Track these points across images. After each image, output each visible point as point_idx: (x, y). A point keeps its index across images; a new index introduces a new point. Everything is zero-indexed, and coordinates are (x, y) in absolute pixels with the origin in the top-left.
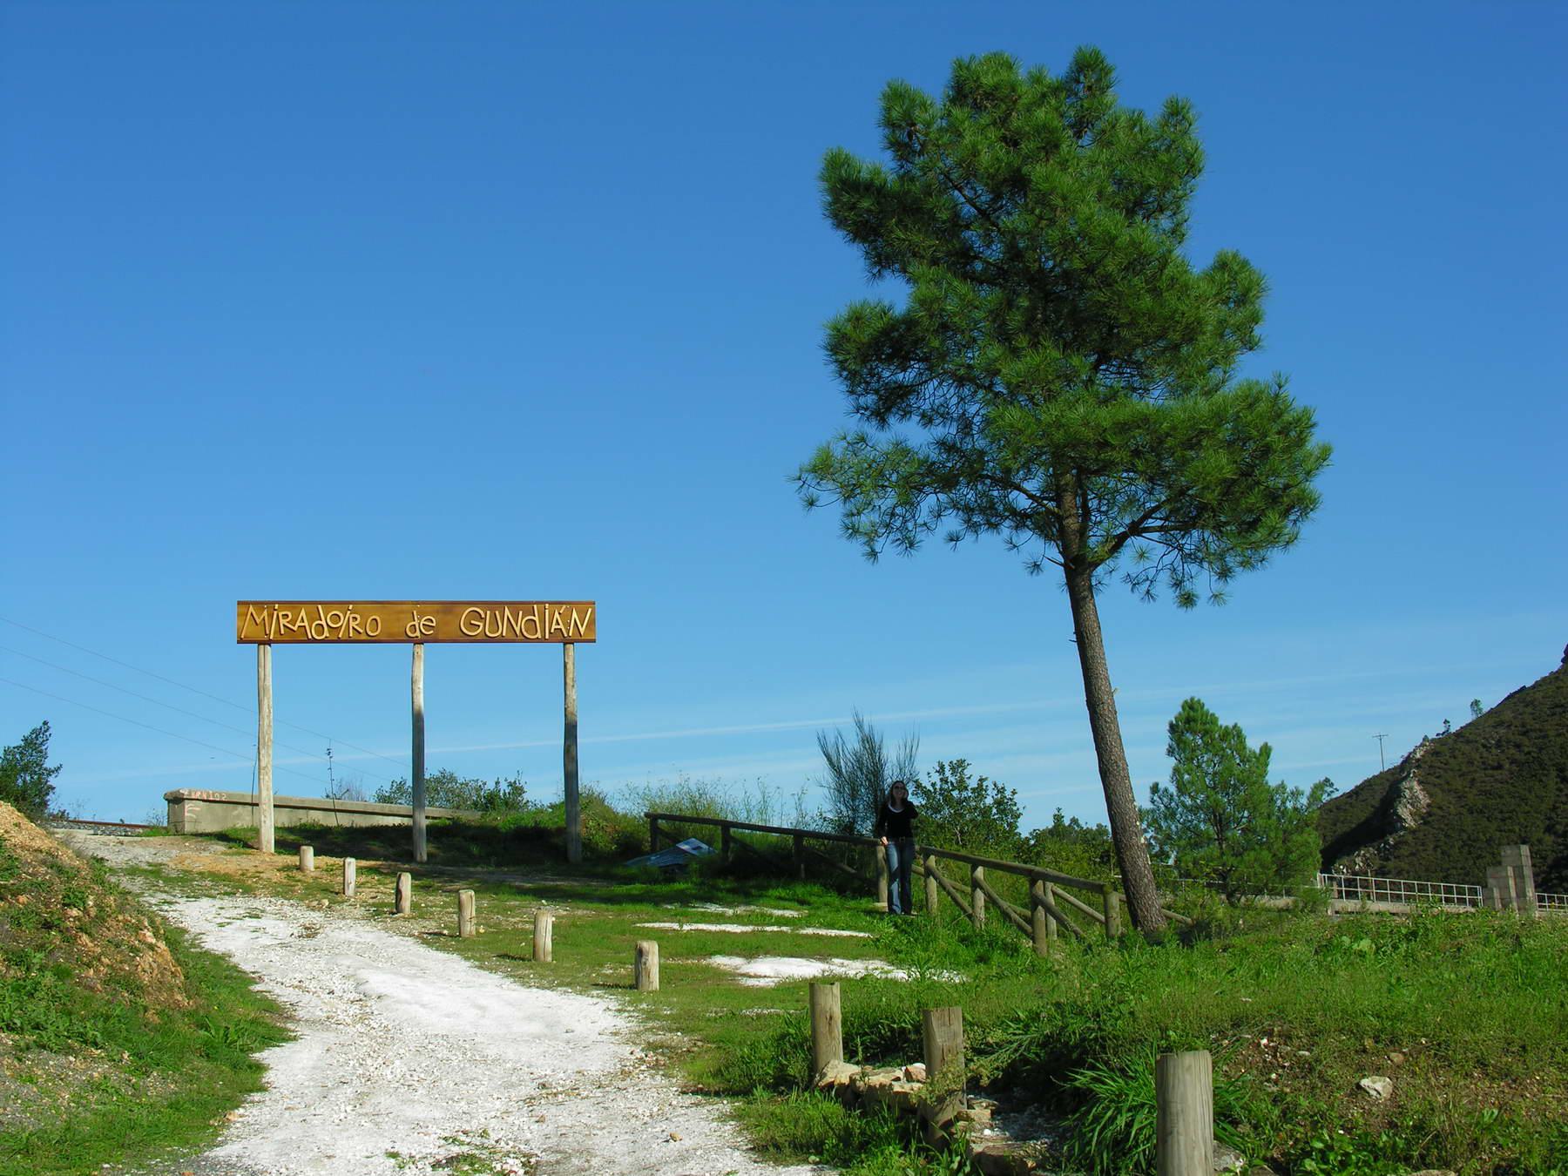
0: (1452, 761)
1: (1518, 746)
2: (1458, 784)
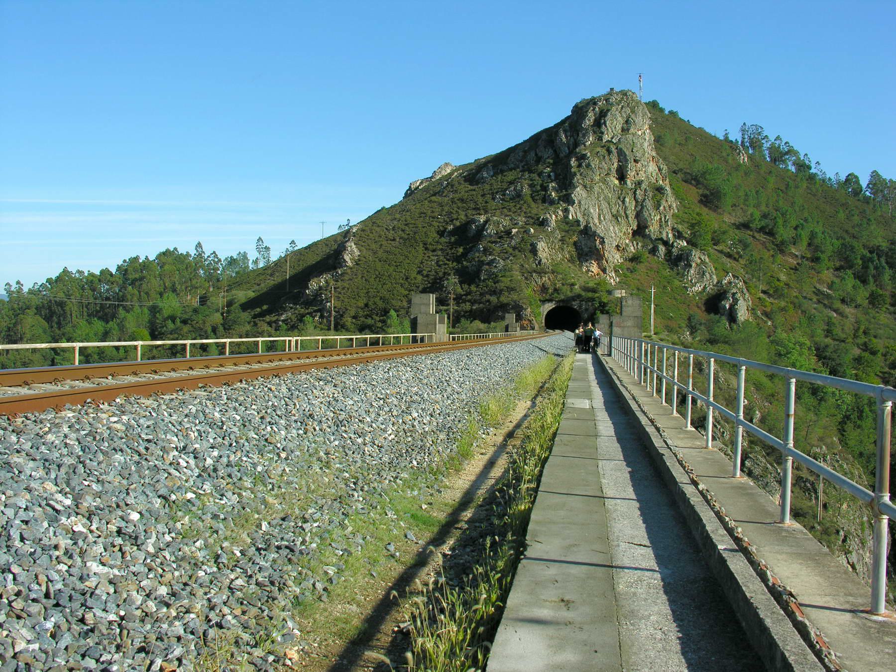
0: (370, 235)
1: (403, 231)
2: (374, 246)
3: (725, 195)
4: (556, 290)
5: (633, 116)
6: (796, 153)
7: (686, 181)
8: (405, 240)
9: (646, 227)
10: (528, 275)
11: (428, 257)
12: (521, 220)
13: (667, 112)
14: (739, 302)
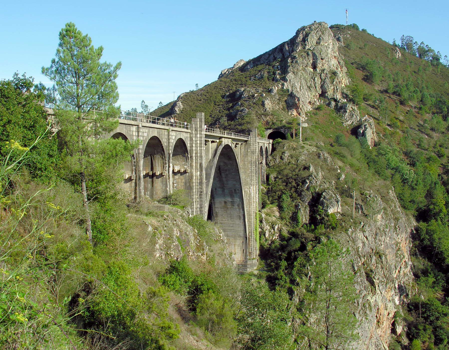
0: (190, 98)
1: (205, 96)
2: (190, 103)
3: (375, 75)
4: (273, 123)
5: (322, 36)
6: (433, 51)
7: (357, 69)
8: (206, 100)
9: (326, 92)
10: (259, 116)
11: (216, 108)
12: (260, 90)
13: (360, 30)
14: (367, 129)
